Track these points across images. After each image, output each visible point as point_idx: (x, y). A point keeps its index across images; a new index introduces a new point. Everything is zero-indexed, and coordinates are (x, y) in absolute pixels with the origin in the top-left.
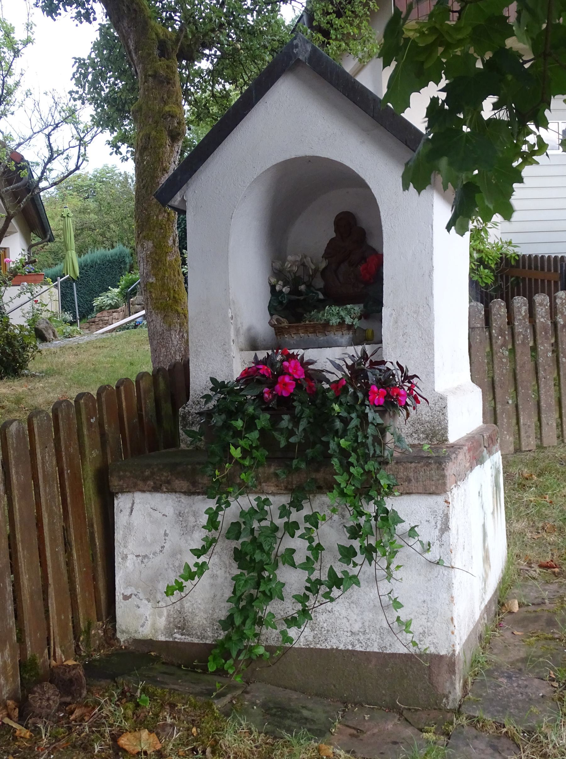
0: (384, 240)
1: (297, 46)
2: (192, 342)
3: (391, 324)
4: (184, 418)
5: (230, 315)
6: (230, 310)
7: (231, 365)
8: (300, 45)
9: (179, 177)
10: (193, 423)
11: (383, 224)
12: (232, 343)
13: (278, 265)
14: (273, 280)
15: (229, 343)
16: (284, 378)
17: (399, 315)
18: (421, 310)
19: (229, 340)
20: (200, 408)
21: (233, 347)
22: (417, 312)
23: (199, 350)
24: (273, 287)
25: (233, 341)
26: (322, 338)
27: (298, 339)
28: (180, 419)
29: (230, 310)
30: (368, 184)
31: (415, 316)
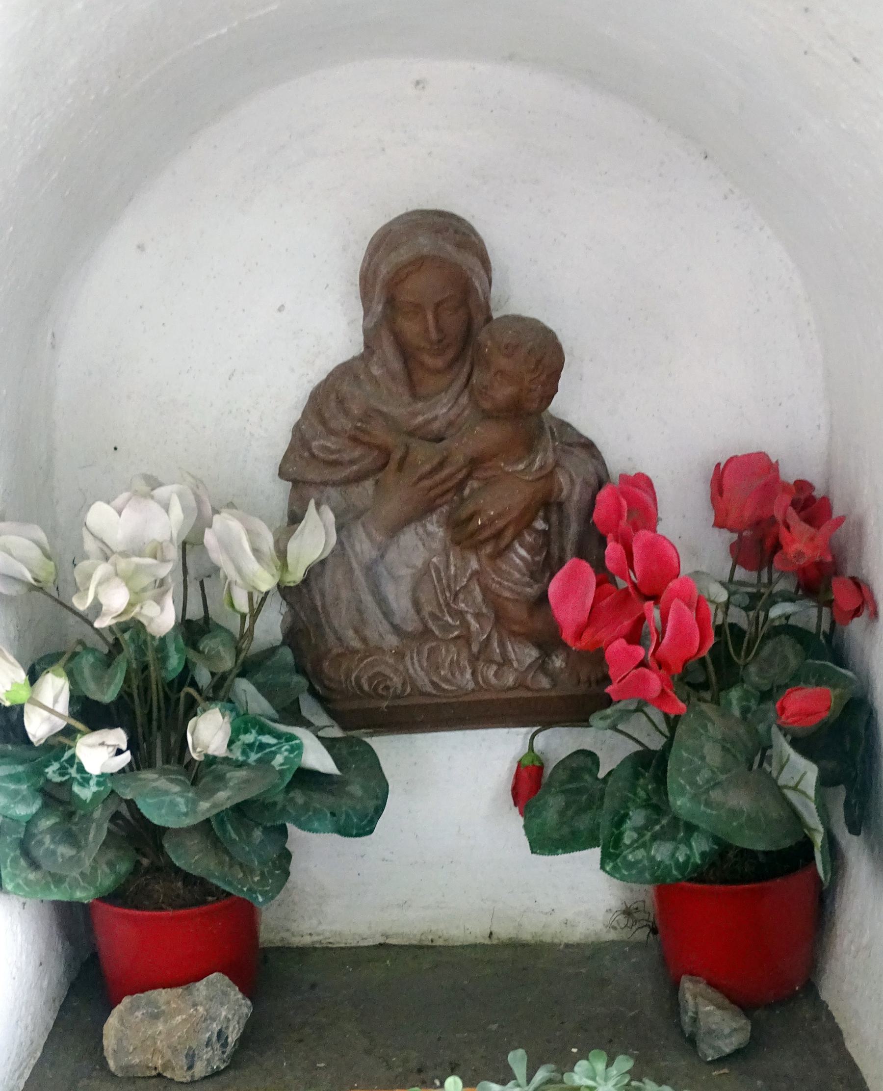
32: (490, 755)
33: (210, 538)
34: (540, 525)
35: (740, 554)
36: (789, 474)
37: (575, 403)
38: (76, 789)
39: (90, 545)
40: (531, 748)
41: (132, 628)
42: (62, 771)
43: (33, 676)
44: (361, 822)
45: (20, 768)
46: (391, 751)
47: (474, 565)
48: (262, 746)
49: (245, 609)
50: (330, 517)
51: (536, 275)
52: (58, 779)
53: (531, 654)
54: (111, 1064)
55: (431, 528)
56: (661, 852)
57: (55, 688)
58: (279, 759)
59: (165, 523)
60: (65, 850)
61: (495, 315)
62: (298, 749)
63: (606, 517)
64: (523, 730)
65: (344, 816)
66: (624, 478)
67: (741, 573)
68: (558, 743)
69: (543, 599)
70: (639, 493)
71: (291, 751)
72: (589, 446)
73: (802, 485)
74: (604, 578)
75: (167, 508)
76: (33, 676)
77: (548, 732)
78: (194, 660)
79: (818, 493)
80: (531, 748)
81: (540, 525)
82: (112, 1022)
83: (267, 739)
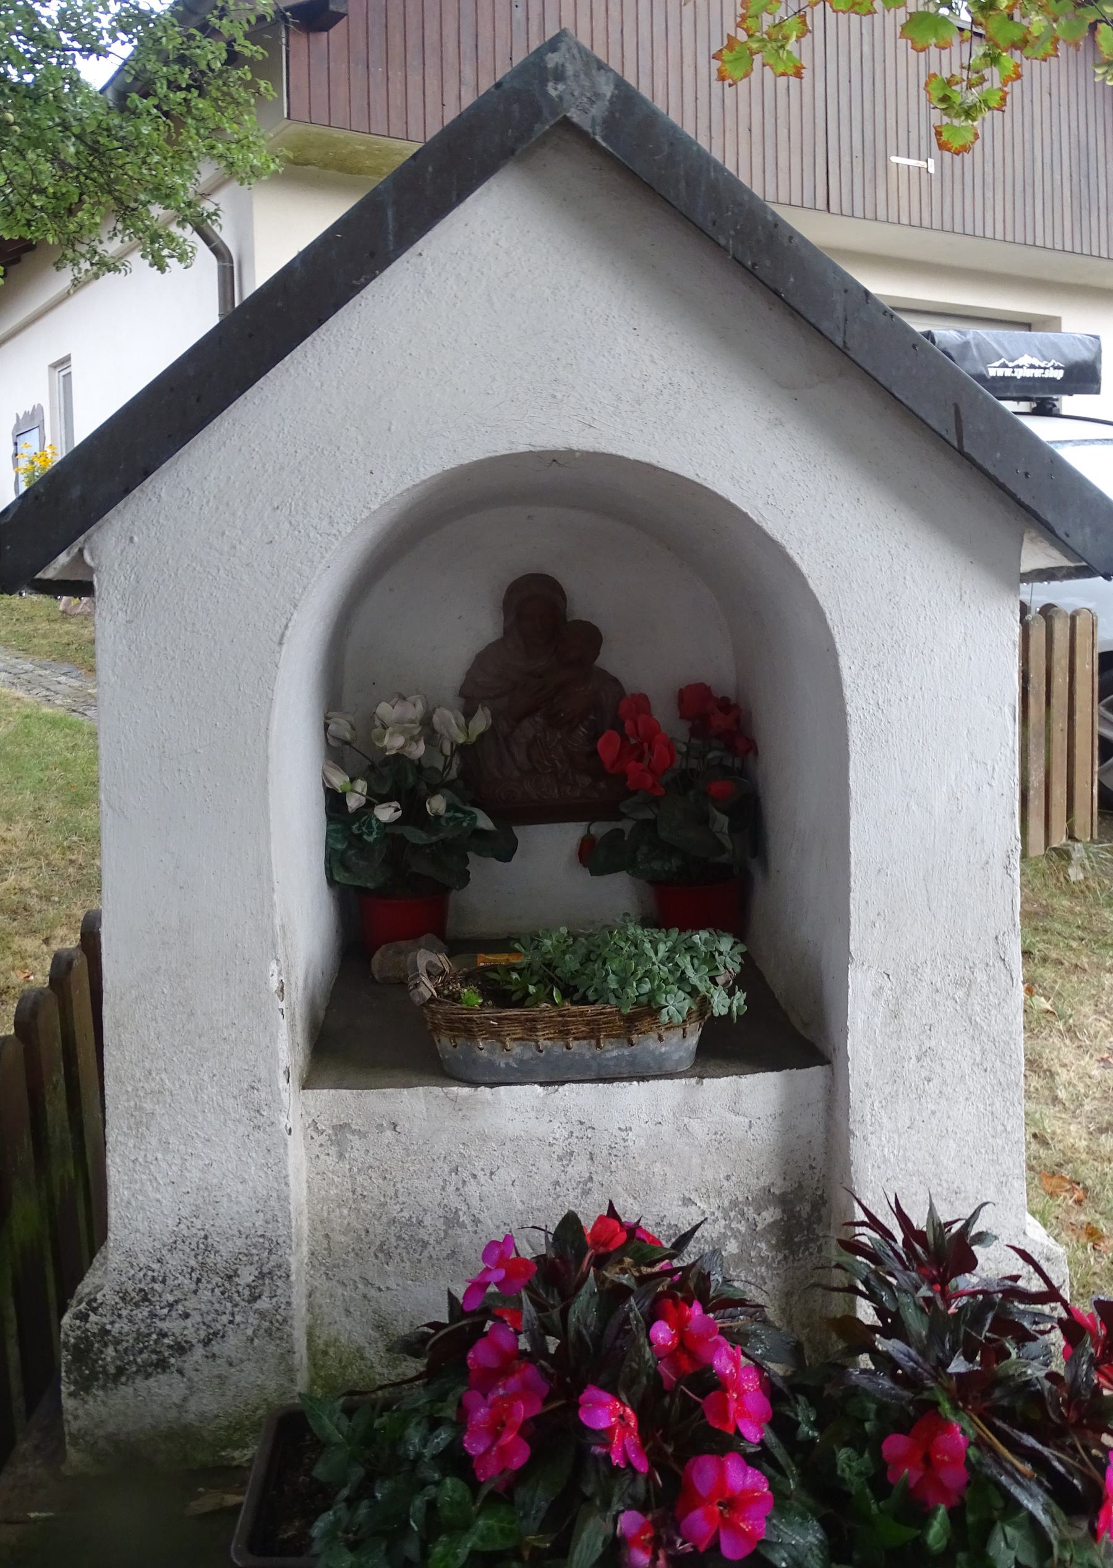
0: (852, 748)
1: (559, 75)
2: (119, 1080)
3: (878, 1021)
4: (83, 1352)
5: (274, 985)
6: (274, 966)
7: (281, 1161)
8: (570, 70)
9: (76, 492)
10: (121, 1371)
11: (848, 693)
12: (282, 1082)
13: (342, 727)
14: (339, 780)
15: (271, 1084)
16: (722, 1470)
17: (904, 992)
18: (980, 977)
19: (272, 1072)
20: (153, 1315)
21: (285, 1096)
22: (966, 984)
23: (148, 1106)
24: (334, 801)
25: (287, 1072)
26: (613, 1051)
27: (528, 1055)
28: (65, 1357)
29: (274, 966)
30: (797, 559)
31: (960, 994)
32: (566, 837)
33: (436, 719)
34: (592, 717)
35: (693, 733)
36: (718, 694)
37: (609, 660)
38: (365, 837)
39: (378, 723)
40: (589, 831)
41: (399, 757)
42: (359, 828)
43: (352, 780)
44: (506, 855)
45: (339, 826)
46: (519, 831)
47: (559, 736)
48: (456, 818)
49: (449, 753)
50: (488, 712)
51: (588, 598)
52: (357, 832)
53: (587, 781)
54: (376, 977)
55: (537, 719)
56: (656, 865)
57: (361, 785)
58: (465, 824)
59: (414, 711)
60: (362, 863)
61: (569, 620)
62: (475, 819)
63: (624, 710)
64: (584, 823)
65: (683, 184)
66: (633, 695)
67: (694, 741)
68: (600, 829)
69: (595, 752)
70: (641, 702)
71: (472, 819)
72: (615, 681)
73: (725, 699)
74: (624, 738)
75: (414, 705)
76: (352, 780)
77: (596, 824)
78: (399, 832)
79: (733, 701)
80: (589, 831)
81: (592, 717)
82: (377, 956)
83: (460, 815)
